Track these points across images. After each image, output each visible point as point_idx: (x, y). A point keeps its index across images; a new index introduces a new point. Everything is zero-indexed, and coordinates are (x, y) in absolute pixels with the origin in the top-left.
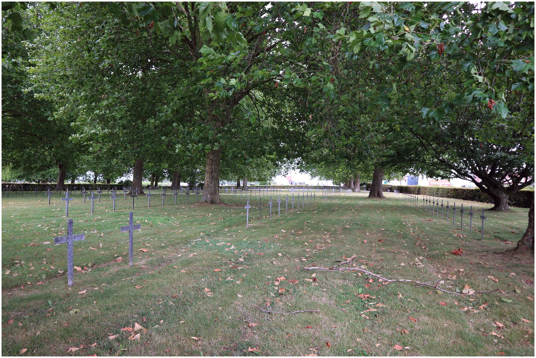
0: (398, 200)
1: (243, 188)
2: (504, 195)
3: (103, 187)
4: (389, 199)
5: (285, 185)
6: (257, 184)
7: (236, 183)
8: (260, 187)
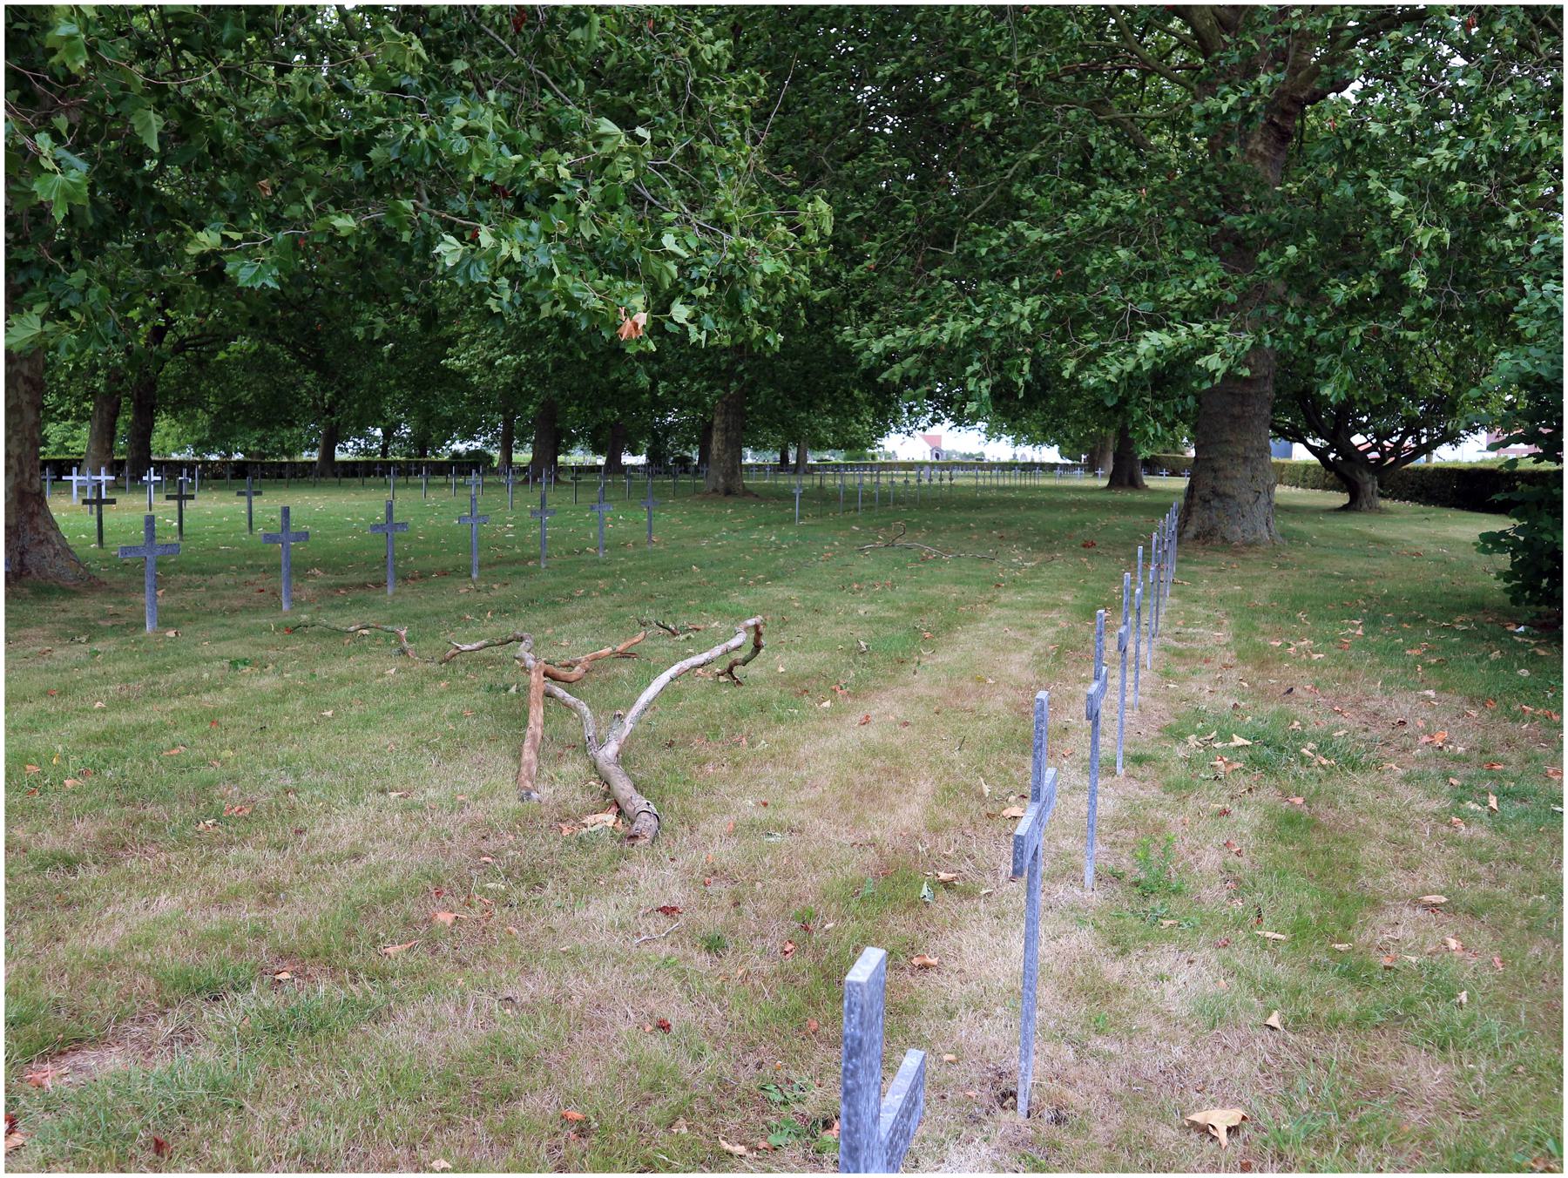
0: (977, 464)
1: (795, 470)
2: (1367, 476)
3: (405, 470)
4: (1153, 491)
5: (919, 459)
6: (835, 457)
7: (778, 456)
8: (846, 466)
